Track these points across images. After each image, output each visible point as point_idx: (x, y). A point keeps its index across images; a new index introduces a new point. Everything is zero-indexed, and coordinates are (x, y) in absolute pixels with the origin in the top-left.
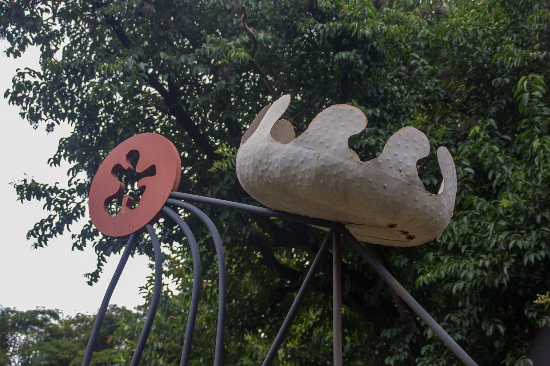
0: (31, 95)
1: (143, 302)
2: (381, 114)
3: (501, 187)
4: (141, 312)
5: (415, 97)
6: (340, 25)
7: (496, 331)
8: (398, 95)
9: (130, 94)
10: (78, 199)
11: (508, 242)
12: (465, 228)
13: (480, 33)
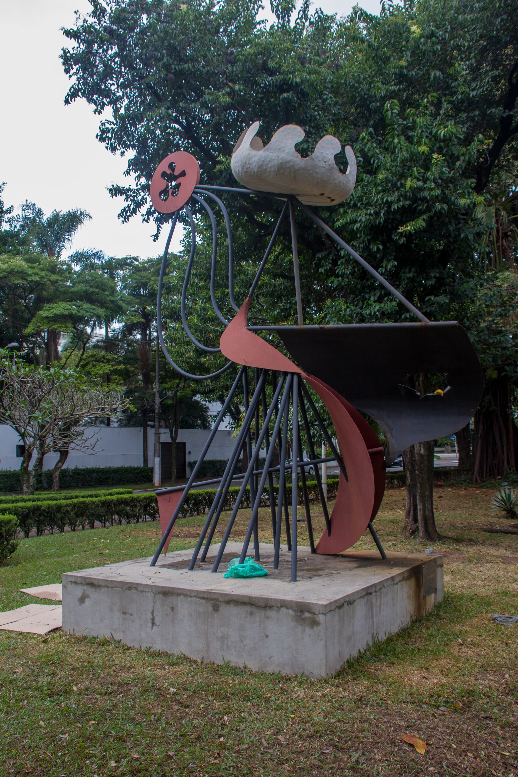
0: (110, 136)
1: (182, 249)
2: (309, 129)
3: (378, 168)
4: (182, 255)
5: (327, 118)
6: (282, 77)
7: (378, 248)
8: (318, 117)
9: (164, 129)
10: (142, 194)
11: (383, 199)
12: (360, 193)
13: (362, 77)
